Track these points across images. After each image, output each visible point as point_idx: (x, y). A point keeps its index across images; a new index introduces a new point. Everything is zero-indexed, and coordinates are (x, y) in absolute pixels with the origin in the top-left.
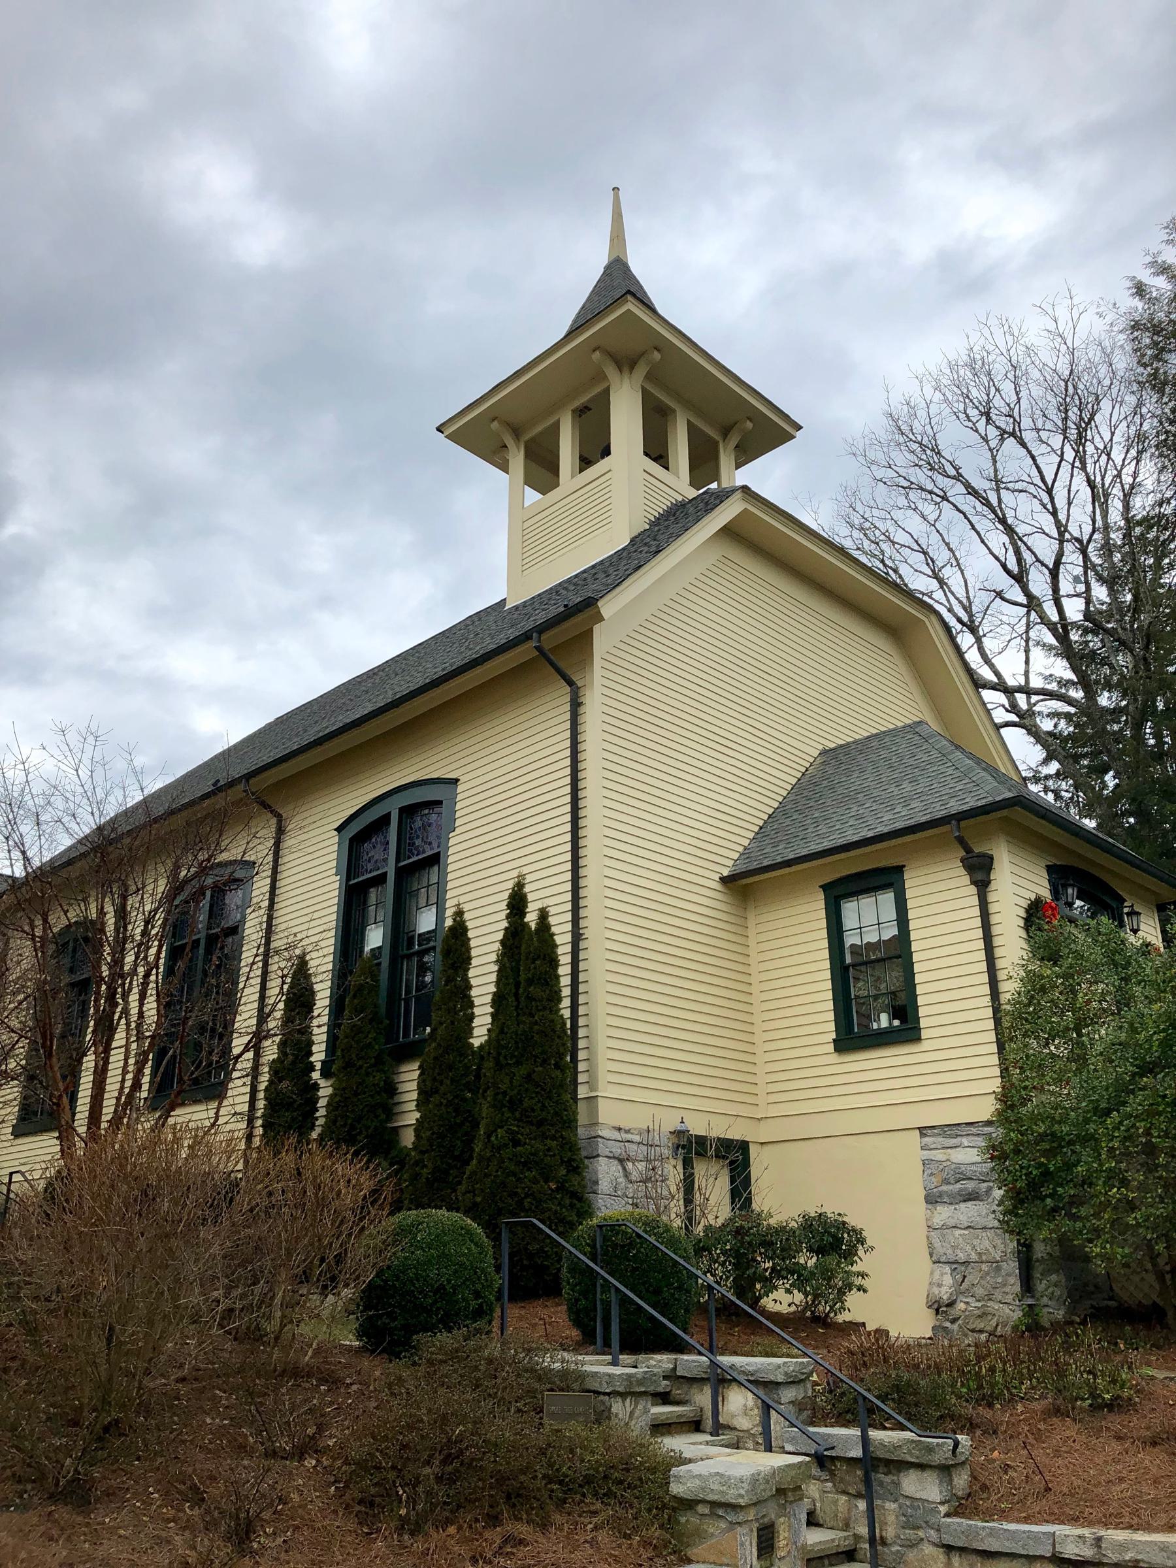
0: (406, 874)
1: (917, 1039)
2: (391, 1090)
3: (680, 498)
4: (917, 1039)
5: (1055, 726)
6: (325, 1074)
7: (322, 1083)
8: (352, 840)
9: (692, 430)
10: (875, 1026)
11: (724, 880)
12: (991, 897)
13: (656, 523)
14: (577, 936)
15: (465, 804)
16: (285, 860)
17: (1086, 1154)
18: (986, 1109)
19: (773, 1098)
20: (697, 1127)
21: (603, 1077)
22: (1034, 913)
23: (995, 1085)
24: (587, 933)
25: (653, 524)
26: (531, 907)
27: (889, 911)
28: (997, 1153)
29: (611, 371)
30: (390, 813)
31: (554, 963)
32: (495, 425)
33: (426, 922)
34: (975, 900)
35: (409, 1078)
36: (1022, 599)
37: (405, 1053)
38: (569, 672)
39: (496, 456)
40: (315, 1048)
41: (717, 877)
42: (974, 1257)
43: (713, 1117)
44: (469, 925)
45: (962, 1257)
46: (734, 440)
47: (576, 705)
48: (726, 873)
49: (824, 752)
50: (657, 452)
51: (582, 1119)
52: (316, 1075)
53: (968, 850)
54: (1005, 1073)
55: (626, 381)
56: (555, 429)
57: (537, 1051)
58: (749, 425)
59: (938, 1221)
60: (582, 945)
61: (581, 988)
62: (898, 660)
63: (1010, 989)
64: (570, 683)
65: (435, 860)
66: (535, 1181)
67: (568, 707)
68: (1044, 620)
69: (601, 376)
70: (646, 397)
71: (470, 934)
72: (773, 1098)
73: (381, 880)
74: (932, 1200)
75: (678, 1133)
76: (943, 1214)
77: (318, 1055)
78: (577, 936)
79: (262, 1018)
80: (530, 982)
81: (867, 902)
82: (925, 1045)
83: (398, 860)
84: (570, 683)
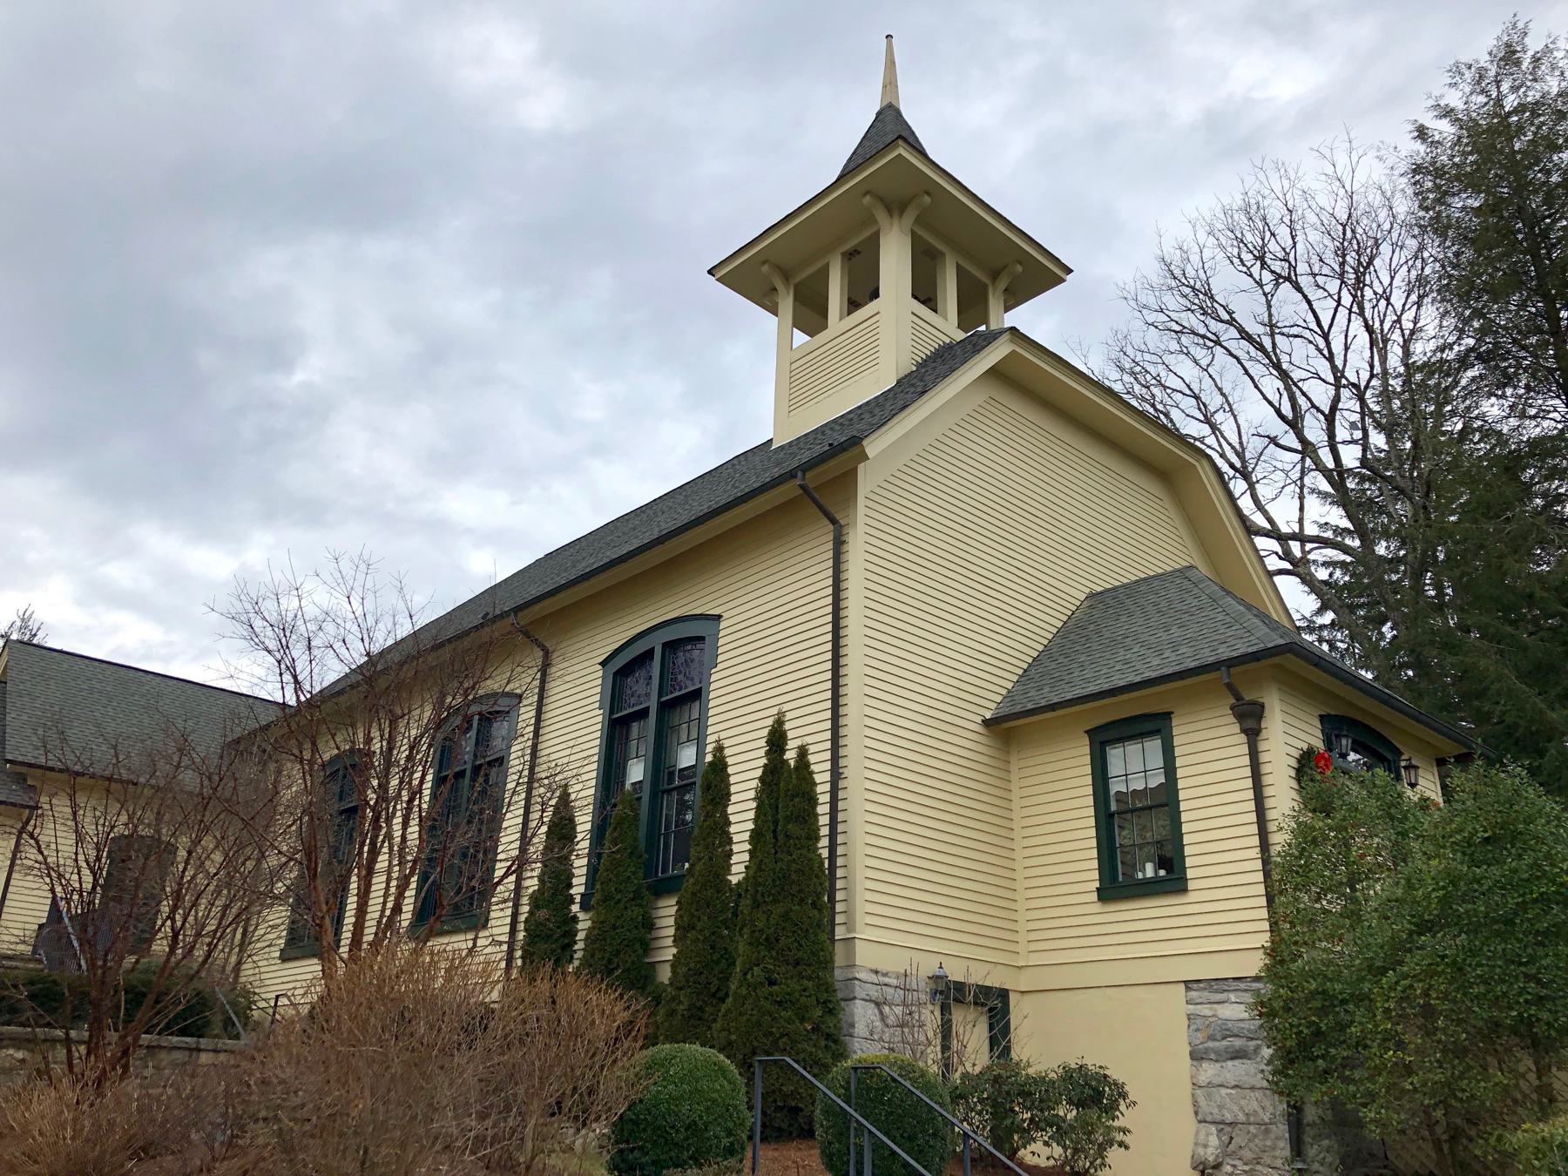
0: (667, 707)
1: (1184, 890)
2: (649, 924)
3: (948, 341)
4: (1184, 890)
5: (1331, 575)
6: (584, 907)
7: (581, 916)
8: (615, 674)
9: (961, 272)
10: (1140, 875)
11: (986, 723)
12: (1262, 746)
13: (923, 365)
14: (836, 775)
15: (728, 640)
16: (553, 669)
17: (1360, 1014)
18: (1254, 964)
19: (1033, 947)
20: (956, 973)
21: (861, 919)
22: (1306, 764)
23: (1264, 939)
24: (846, 772)
25: (919, 365)
26: (791, 744)
27: (1158, 761)
28: (1266, 1010)
29: (881, 216)
30: (652, 650)
31: (813, 801)
32: (765, 268)
33: (686, 757)
34: (1245, 749)
35: (667, 913)
36: (1297, 446)
37: (662, 888)
38: (832, 510)
39: (765, 298)
40: (575, 881)
41: (979, 720)
42: (1242, 1118)
43: (943, 959)
44: (730, 761)
45: (1229, 1117)
46: (1003, 283)
47: (839, 545)
48: (988, 715)
49: (1091, 596)
50: (925, 293)
51: (839, 960)
52: (575, 908)
53: (1238, 697)
54: (1274, 927)
55: (896, 228)
56: (824, 274)
57: (795, 889)
58: (1019, 268)
59: (1203, 1078)
60: (841, 784)
61: (840, 828)
62: (1167, 503)
63: (1279, 840)
64: (833, 521)
65: (697, 695)
66: (789, 1021)
67: (830, 545)
68: (1320, 467)
69: (873, 220)
70: (914, 236)
71: (730, 770)
72: (1033, 947)
73: (643, 714)
74: (1197, 1056)
75: (935, 978)
76: (1209, 1071)
77: (578, 888)
78: (836, 775)
79: (525, 841)
80: (788, 819)
81: (1133, 748)
82: (1192, 897)
83: (660, 695)
84: (833, 521)
